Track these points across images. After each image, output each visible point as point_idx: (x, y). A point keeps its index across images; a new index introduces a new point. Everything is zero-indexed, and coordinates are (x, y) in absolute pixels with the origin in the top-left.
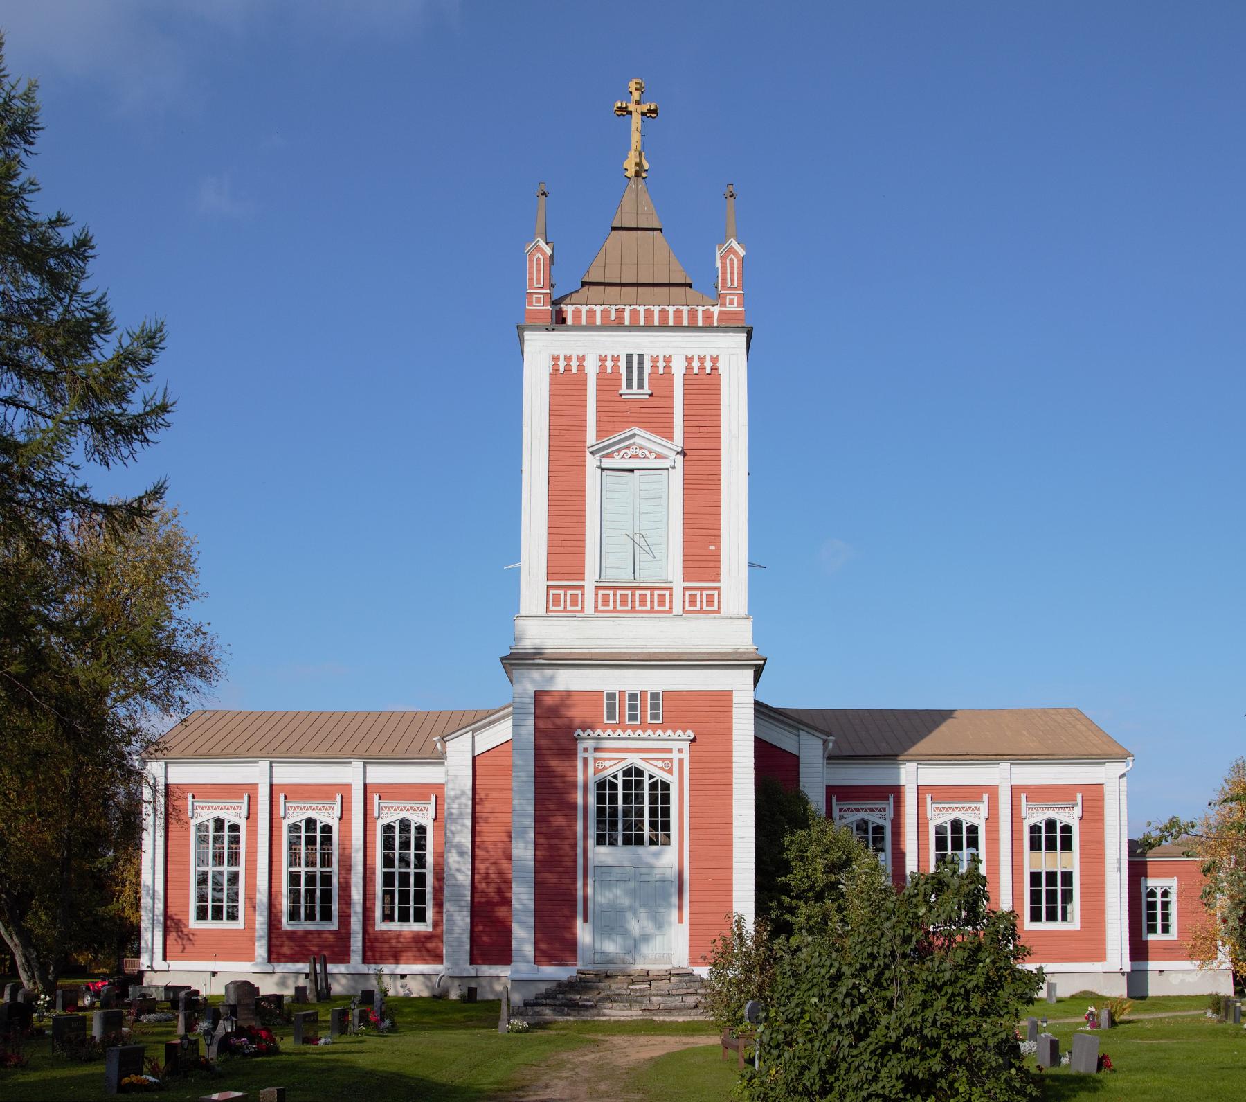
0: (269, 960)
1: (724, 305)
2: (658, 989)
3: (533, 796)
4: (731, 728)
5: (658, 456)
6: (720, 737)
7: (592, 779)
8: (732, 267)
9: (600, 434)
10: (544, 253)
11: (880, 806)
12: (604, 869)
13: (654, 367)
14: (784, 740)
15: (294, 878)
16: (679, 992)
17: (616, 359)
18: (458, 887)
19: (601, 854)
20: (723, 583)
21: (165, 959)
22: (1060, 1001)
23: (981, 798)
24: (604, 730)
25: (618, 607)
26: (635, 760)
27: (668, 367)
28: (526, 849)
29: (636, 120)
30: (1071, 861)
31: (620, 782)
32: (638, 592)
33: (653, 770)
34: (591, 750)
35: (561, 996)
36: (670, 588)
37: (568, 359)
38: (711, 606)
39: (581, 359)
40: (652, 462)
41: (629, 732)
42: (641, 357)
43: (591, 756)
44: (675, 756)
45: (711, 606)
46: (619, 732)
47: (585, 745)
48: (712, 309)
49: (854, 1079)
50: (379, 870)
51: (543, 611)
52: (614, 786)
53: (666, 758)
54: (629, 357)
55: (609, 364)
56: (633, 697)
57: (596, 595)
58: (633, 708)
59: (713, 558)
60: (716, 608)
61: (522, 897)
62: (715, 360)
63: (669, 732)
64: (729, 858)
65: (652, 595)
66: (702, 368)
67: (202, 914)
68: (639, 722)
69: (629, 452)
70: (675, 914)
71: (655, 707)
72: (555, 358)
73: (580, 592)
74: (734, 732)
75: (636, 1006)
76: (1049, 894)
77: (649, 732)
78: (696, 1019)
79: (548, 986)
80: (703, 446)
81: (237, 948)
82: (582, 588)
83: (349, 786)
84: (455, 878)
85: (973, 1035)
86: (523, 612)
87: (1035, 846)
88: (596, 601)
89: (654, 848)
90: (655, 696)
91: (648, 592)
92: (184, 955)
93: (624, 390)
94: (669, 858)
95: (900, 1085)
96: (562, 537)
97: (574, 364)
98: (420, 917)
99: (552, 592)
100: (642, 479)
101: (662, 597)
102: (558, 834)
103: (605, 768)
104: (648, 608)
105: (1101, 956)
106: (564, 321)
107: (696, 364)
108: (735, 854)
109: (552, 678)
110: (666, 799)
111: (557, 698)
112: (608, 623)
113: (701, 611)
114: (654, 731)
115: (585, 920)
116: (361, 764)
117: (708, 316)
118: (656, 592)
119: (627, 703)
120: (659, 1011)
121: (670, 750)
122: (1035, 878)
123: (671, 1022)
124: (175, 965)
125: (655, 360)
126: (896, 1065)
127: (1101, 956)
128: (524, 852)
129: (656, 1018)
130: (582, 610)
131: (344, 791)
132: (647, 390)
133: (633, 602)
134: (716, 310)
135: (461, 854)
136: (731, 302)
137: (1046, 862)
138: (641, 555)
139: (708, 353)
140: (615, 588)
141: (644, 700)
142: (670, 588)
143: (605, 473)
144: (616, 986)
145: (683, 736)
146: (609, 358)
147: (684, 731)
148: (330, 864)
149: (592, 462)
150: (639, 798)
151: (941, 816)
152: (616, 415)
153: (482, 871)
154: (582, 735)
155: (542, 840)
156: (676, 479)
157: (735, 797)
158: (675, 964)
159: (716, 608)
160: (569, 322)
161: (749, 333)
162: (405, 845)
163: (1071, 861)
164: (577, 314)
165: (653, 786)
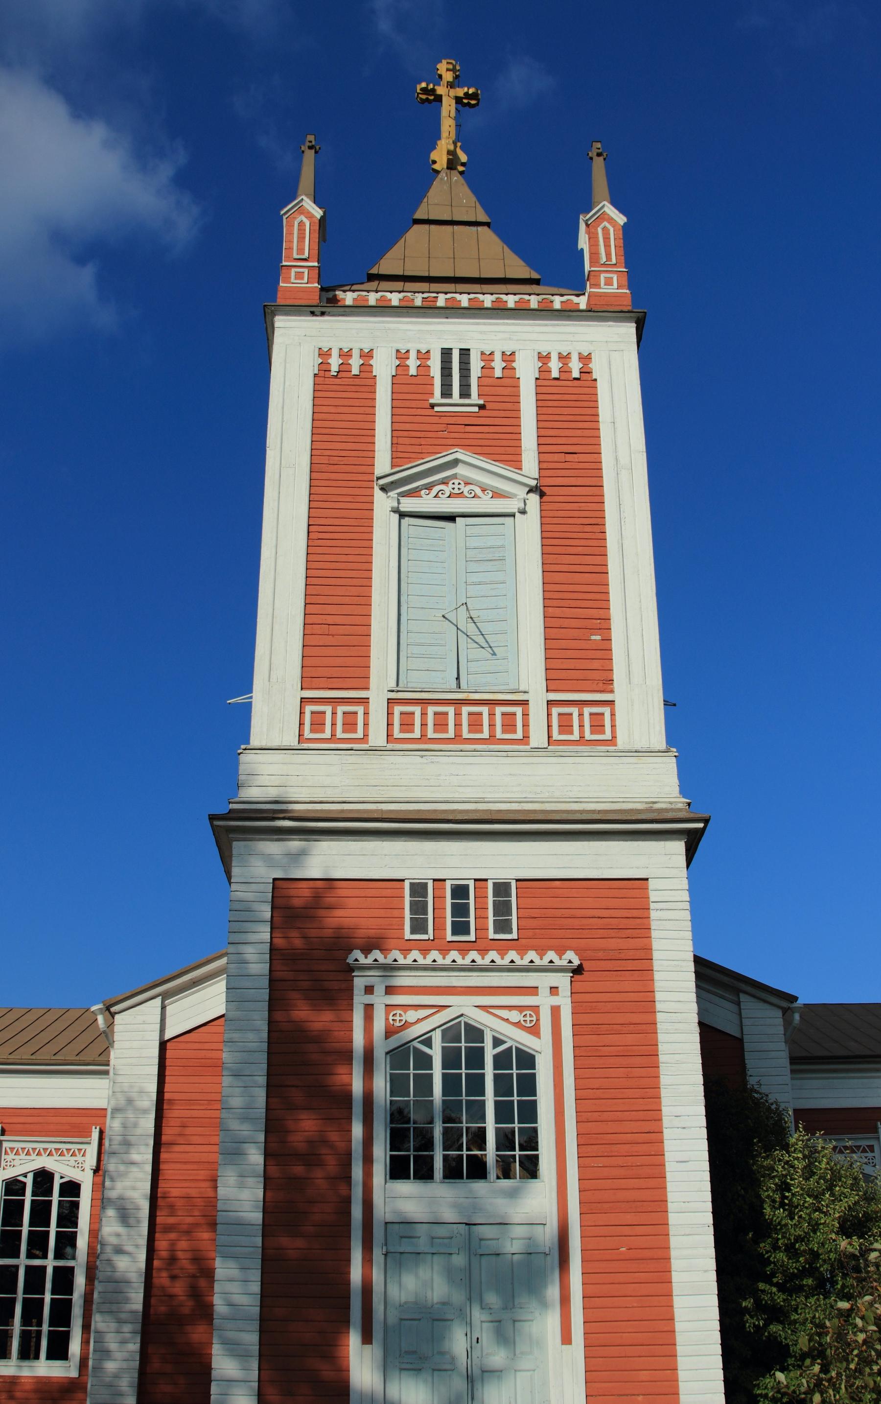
5: (497, 494)
6: (630, 965)
8: (607, 239)
9: (398, 457)
10: (310, 216)
11: (864, 1143)
13: (487, 368)
17: (424, 356)
18: (119, 1284)
19: (402, 1200)
24: (405, 951)
25: (431, 734)
26: (466, 1008)
28: (241, 1186)
29: (448, 107)
32: (465, 710)
33: (501, 1027)
34: (379, 989)
36: (524, 703)
37: (346, 355)
38: (600, 736)
40: (486, 504)
41: (454, 955)
42: (465, 353)
44: (544, 1001)
45: (600, 736)
46: (434, 955)
51: (291, 740)
52: (425, 1061)
53: (526, 1009)
54: (446, 353)
56: (460, 891)
57: (390, 714)
58: (460, 910)
59: (599, 654)
60: (608, 735)
61: (236, 1288)
62: (585, 359)
63: (532, 955)
64: (658, 1204)
65: (492, 715)
68: (472, 937)
69: (447, 489)
70: (552, 1321)
71: (503, 908)
72: (324, 354)
73: (360, 710)
74: (656, 955)
80: (573, 481)
82: (365, 701)
84: (114, 1269)
86: (255, 741)
89: (505, 1183)
90: (502, 888)
91: (485, 710)
93: (437, 398)
94: (535, 1206)
96: (330, 619)
98: (58, 1351)
99: (309, 709)
100: (471, 531)
101: (509, 718)
102: (310, 1157)
103: (406, 1025)
104: (486, 734)
108: (671, 1197)
109: (303, 853)
110: (528, 1085)
112: (414, 759)
113: (582, 741)
114: (502, 953)
115: (367, 1338)
118: (499, 710)
119: (449, 901)
121: (533, 990)
125: (487, 357)
128: (242, 1194)
132: (475, 398)
133: (458, 725)
135: (125, 1216)
138: (469, 651)
139: (575, 349)
140: (424, 703)
141: (481, 897)
142: (524, 703)
143: (406, 521)
146: (413, 355)
147: (561, 952)
150: (477, 1085)
152: (424, 431)
153: (164, 1254)
156: (528, 531)
159: (608, 735)
162: (41, 1213)
165: (501, 1061)
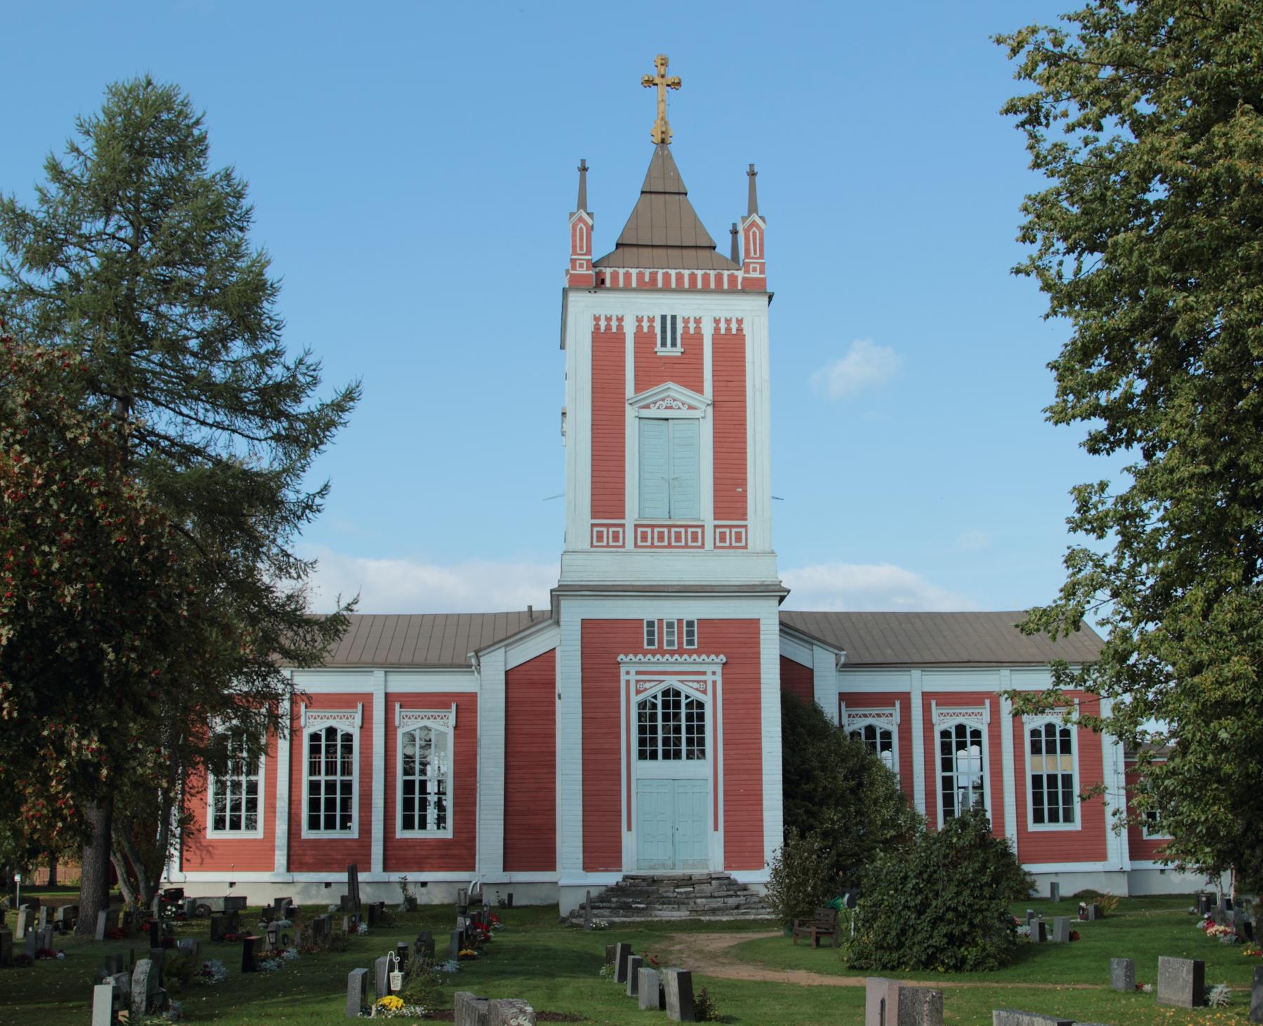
0: (289, 870)
1: (747, 271)
2: (701, 891)
4: (759, 653)
5: (691, 407)
9: (638, 389)
11: (887, 712)
13: (686, 328)
14: (801, 655)
15: (314, 787)
17: (651, 320)
20: (750, 522)
21: (181, 870)
22: (1063, 899)
23: (983, 704)
26: (673, 682)
27: (698, 328)
30: (1070, 764)
31: (659, 703)
32: (673, 530)
33: (689, 690)
35: (614, 900)
36: (702, 527)
39: (620, 320)
40: (685, 413)
42: (674, 318)
44: (709, 678)
48: (736, 273)
49: (919, 937)
50: (400, 779)
51: (587, 546)
52: (654, 706)
53: (702, 680)
54: (664, 318)
55: (645, 324)
57: (636, 532)
60: (743, 544)
62: (740, 322)
66: (728, 329)
67: (219, 824)
69: (664, 404)
71: (690, 633)
72: (597, 319)
76: (1049, 796)
78: (738, 918)
81: (258, 857)
82: (623, 526)
83: (371, 695)
85: (986, 910)
87: (1036, 749)
88: (636, 538)
90: (690, 624)
92: (202, 866)
95: (945, 940)
97: (614, 324)
103: (646, 689)
105: (1101, 856)
106: (603, 282)
107: (723, 326)
113: (731, 547)
116: (382, 674)
117: (733, 279)
120: (705, 912)
122: (1037, 780)
123: (716, 922)
124: (192, 876)
125: (686, 321)
126: (943, 929)
127: (1101, 856)
130: (623, 546)
131: (366, 700)
134: (740, 274)
136: (754, 270)
137: (1045, 765)
140: (652, 526)
142: (702, 527)
145: (716, 660)
148: (350, 774)
149: (630, 413)
151: (945, 720)
152: (652, 372)
160: (608, 283)
161: (770, 298)
163: (1070, 764)
164: (615, 276)
165: (689, 705)
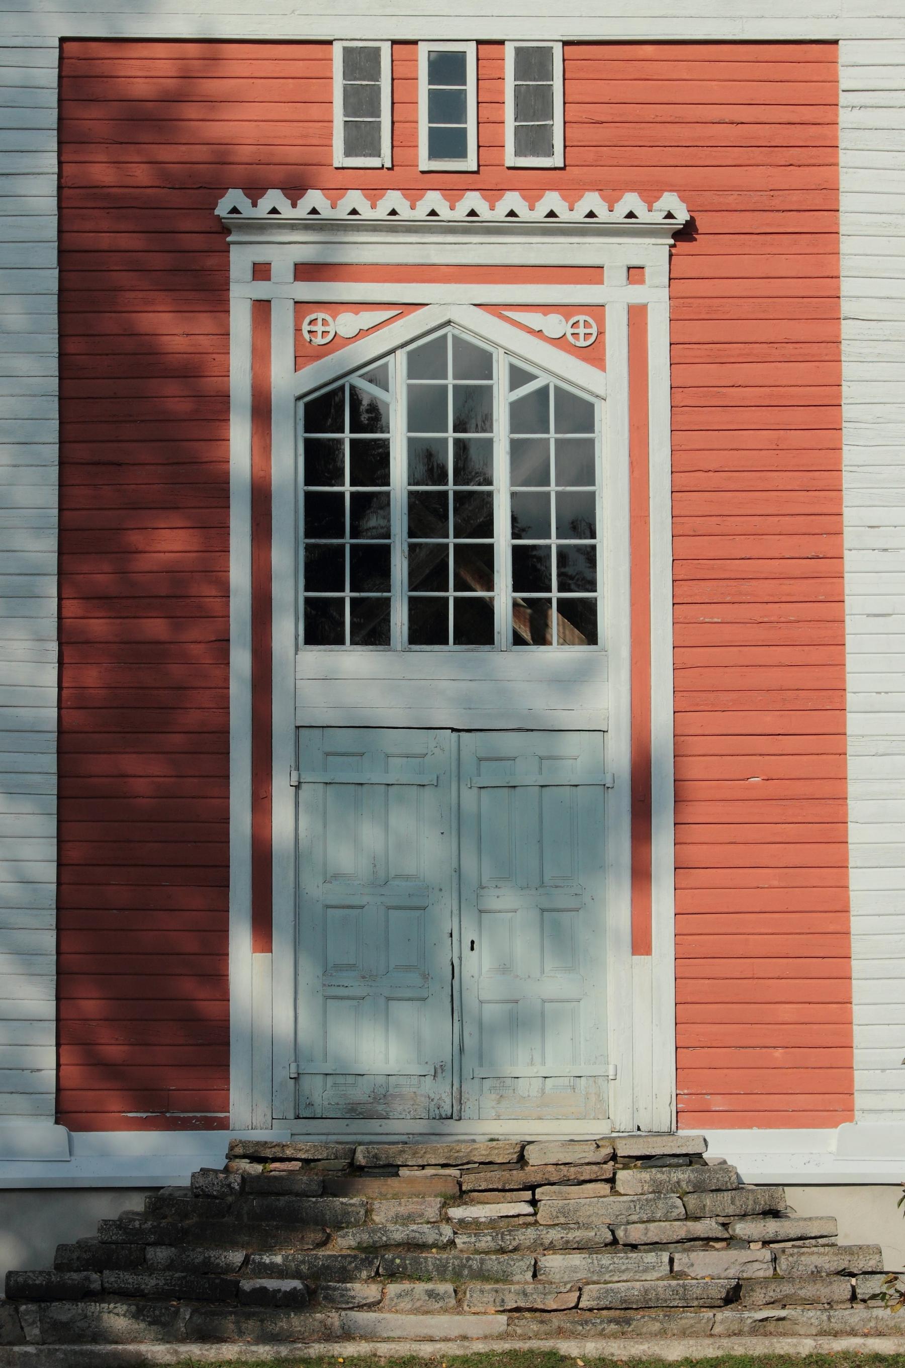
3: (52, 452)
6: (793, 222)
7: (288, 381)
12: (344, 740)
16: (655, 1232)
24: (336, 192)
26: (456, 307)
33: (525, 347)
35: (160, 1254)
41: (433, 199)
43: (285, 290)
44: (615, 295)
46: (394, 199)
47: (264, 259)
52: (371, 417)
56: (447, 66)
58: (447, 106)
63: (592, 201)
70: (618, 909)
71: (534, 103)
74: (846, 202)
75: (479, 1294)
77: (512, 200)
79: (105, 1209)
90: (533, 61)
94: (604, 696)
103: (337, 343)
111: (166, 68)
121: (592, 273)
129: (568, 1347)
141: (489, 78)
144: (391, 1210)
147: (650, 196)
154: (247, 210)
155: (99, 626)
157: (849, 455)
158: (623, 1120)
165: (530, 413)
